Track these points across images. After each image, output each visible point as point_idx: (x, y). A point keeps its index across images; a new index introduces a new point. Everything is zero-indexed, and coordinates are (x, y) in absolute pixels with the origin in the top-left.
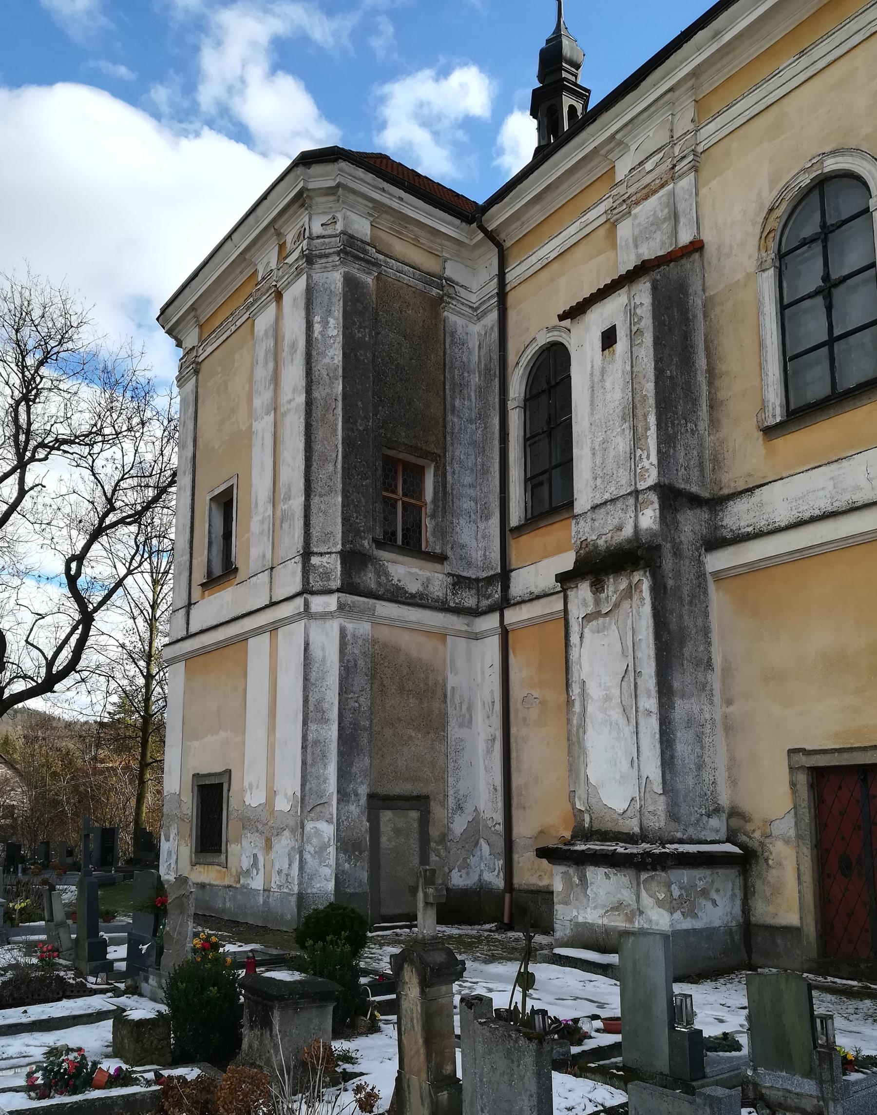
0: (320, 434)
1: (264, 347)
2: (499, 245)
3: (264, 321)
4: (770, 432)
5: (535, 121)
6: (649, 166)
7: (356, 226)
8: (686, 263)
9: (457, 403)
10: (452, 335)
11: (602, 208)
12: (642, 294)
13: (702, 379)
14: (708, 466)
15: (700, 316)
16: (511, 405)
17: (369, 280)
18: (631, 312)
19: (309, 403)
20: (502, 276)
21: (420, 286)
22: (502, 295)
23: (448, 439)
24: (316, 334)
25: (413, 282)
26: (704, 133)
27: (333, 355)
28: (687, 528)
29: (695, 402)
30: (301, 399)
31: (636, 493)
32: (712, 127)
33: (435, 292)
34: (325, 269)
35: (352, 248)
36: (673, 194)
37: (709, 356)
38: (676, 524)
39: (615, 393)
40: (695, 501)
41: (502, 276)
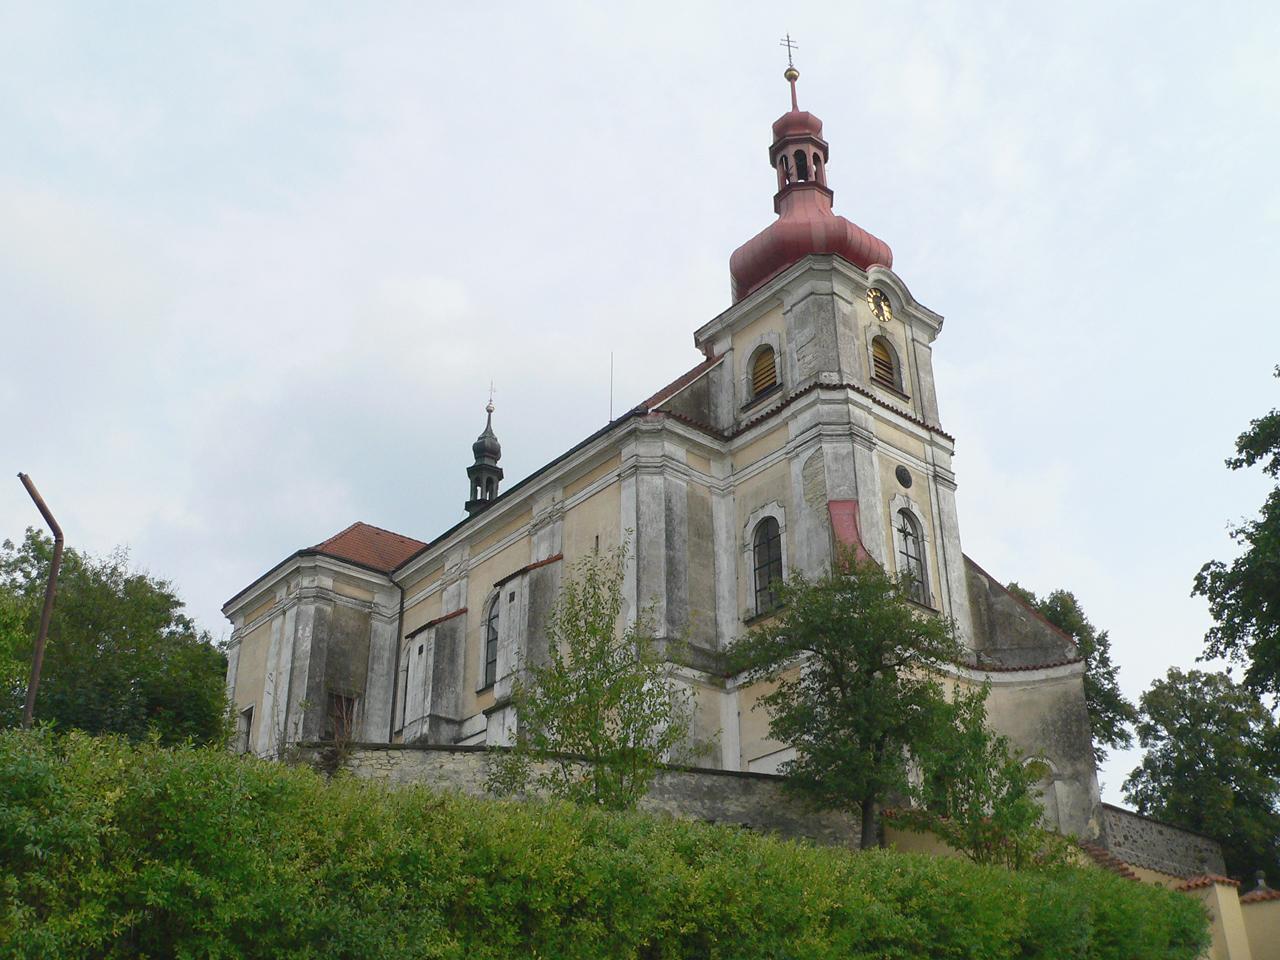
0: (296, 684)
1: (276, 636)
2: (400, 588)
3: (277, 623)
4: (479, 693)
5: (775, 171)
6: (453, 570)
7: (324, 583)
8: (458, 619)
9: (375, 667)
10: (375, 631)
11: (439, 582)
12: (432, 633)
13: (461, 668)
14: (460, 706)
15: (463, 640)
16: (400, 669)
17: (329, 609)
18: (428, 639)
19: (292, 669)
20: (402, 603)
21: (359, 608)
22: (401, 613)
23: (368, 685)
24: (299, 635)
25: (354, 606)
26: (567, 502)
27: (306, 646)
28: (444, 733)
29: (455, 679)
30: (289, 666)
31: (423, 717)
32: (474, 560)
33: (367, 610)
34: (306, 604)
35: (321, 595)
36: (459, 585)
37: (465, 658)
38: (438, 731)
39: (421, 675)
40: (449, 721)
41: (402, 603)
